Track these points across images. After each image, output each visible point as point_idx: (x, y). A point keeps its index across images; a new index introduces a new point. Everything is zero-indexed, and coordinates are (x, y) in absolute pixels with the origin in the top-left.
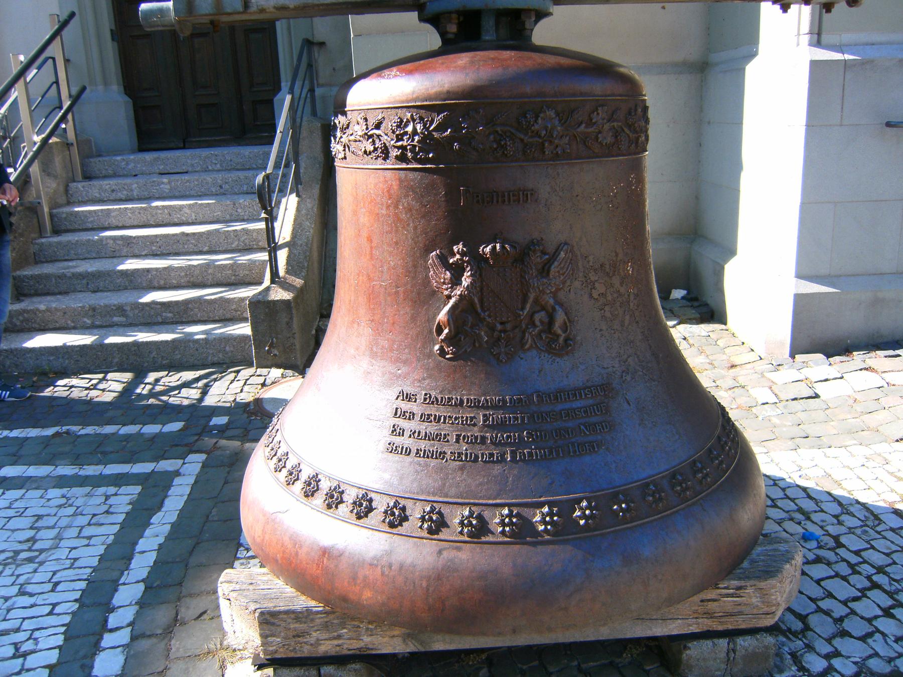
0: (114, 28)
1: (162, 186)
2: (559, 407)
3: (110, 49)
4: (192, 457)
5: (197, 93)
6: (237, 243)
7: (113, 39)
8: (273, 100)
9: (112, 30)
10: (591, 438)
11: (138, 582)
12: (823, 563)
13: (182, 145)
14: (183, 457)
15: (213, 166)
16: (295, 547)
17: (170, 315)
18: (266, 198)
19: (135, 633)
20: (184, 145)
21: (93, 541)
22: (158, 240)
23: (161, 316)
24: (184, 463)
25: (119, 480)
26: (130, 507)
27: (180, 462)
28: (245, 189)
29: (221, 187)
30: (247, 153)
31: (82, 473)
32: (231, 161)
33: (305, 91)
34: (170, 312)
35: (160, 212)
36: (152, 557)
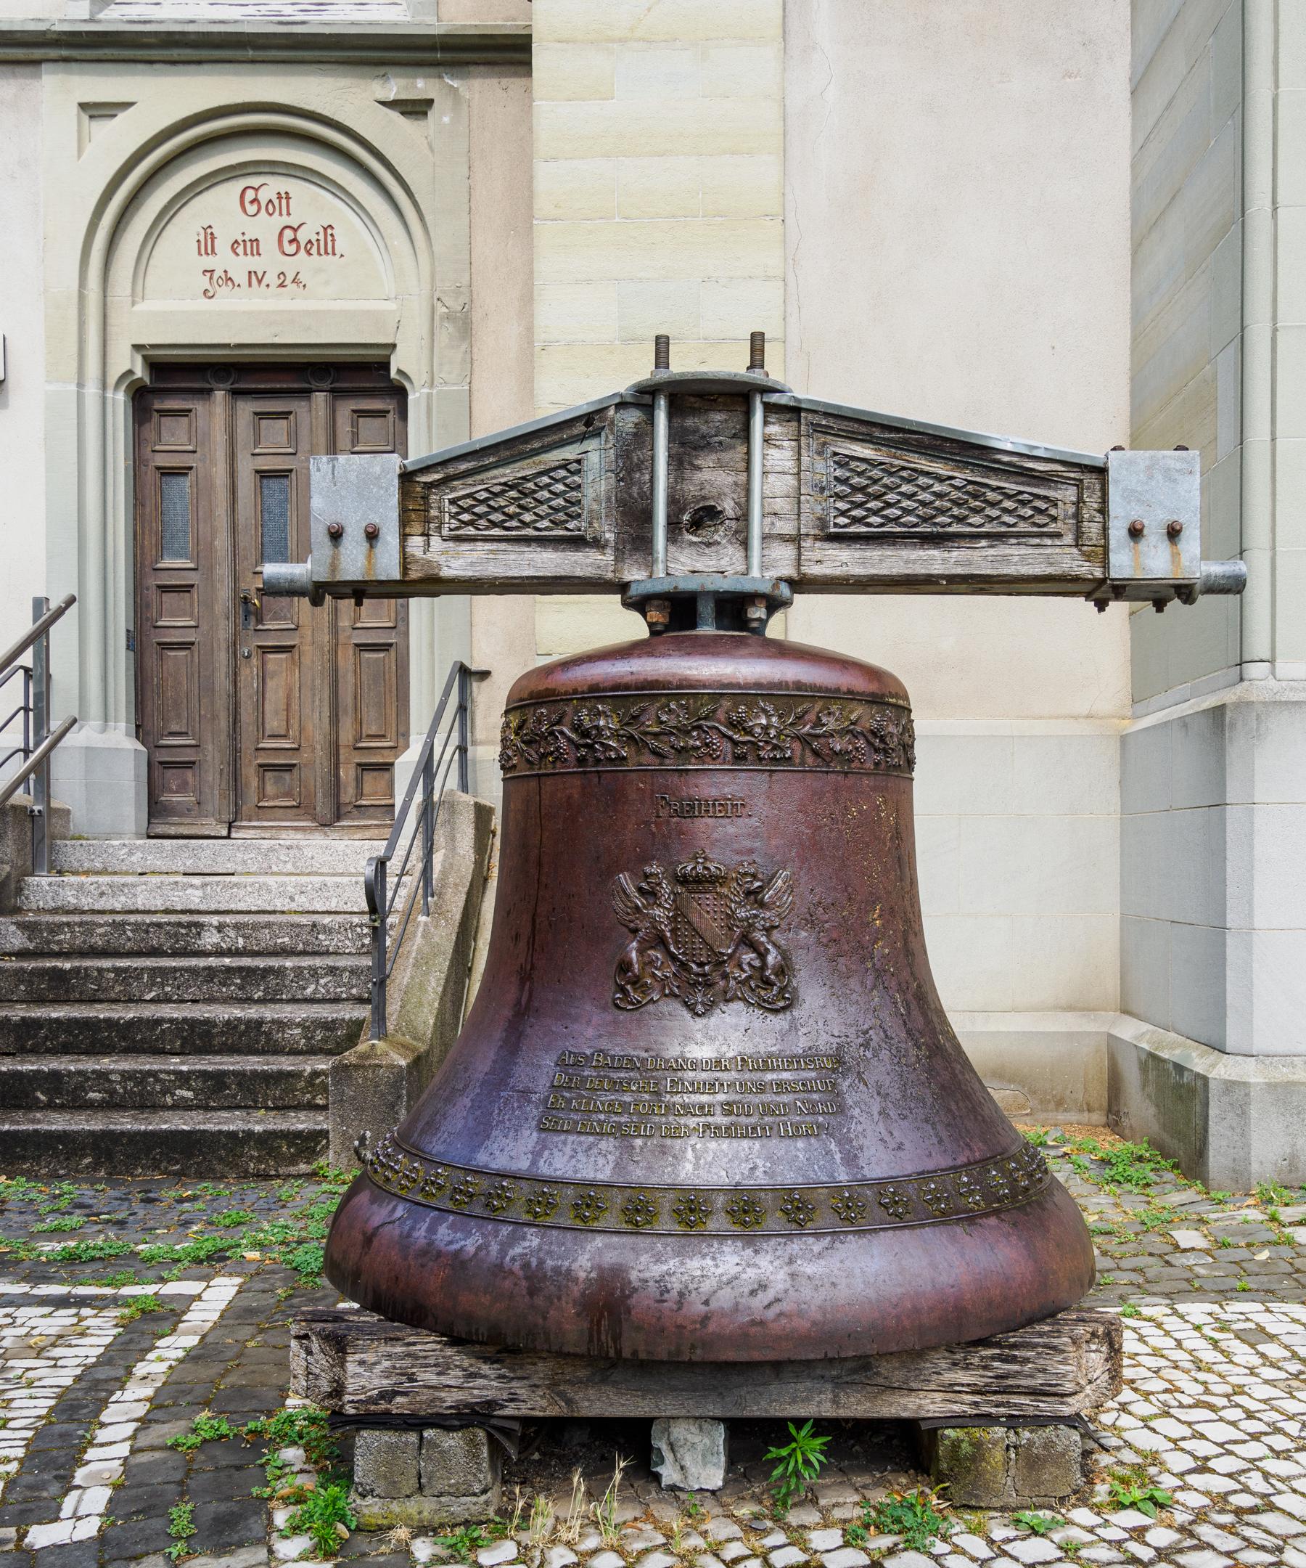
0: (132, 629)
3: (121, 660)
5: (261, 745)
6: (313, 986)
7: (128, 648)
8: (392, 764)
9: (128, 631)
12: (645, 617)
14: (207, 1278)
15: (281, 865)
16: (406, 1259)
17: (190, 1094)
20: (229, 832)
21: (60, 1363)
23: (173, 1094)
24: (208, 1286)
25: (98, 1303)
29: (292, 899)
31: (35, 1292)
33: (450, 750)
34: (188, 1089)
35: (183, 931)
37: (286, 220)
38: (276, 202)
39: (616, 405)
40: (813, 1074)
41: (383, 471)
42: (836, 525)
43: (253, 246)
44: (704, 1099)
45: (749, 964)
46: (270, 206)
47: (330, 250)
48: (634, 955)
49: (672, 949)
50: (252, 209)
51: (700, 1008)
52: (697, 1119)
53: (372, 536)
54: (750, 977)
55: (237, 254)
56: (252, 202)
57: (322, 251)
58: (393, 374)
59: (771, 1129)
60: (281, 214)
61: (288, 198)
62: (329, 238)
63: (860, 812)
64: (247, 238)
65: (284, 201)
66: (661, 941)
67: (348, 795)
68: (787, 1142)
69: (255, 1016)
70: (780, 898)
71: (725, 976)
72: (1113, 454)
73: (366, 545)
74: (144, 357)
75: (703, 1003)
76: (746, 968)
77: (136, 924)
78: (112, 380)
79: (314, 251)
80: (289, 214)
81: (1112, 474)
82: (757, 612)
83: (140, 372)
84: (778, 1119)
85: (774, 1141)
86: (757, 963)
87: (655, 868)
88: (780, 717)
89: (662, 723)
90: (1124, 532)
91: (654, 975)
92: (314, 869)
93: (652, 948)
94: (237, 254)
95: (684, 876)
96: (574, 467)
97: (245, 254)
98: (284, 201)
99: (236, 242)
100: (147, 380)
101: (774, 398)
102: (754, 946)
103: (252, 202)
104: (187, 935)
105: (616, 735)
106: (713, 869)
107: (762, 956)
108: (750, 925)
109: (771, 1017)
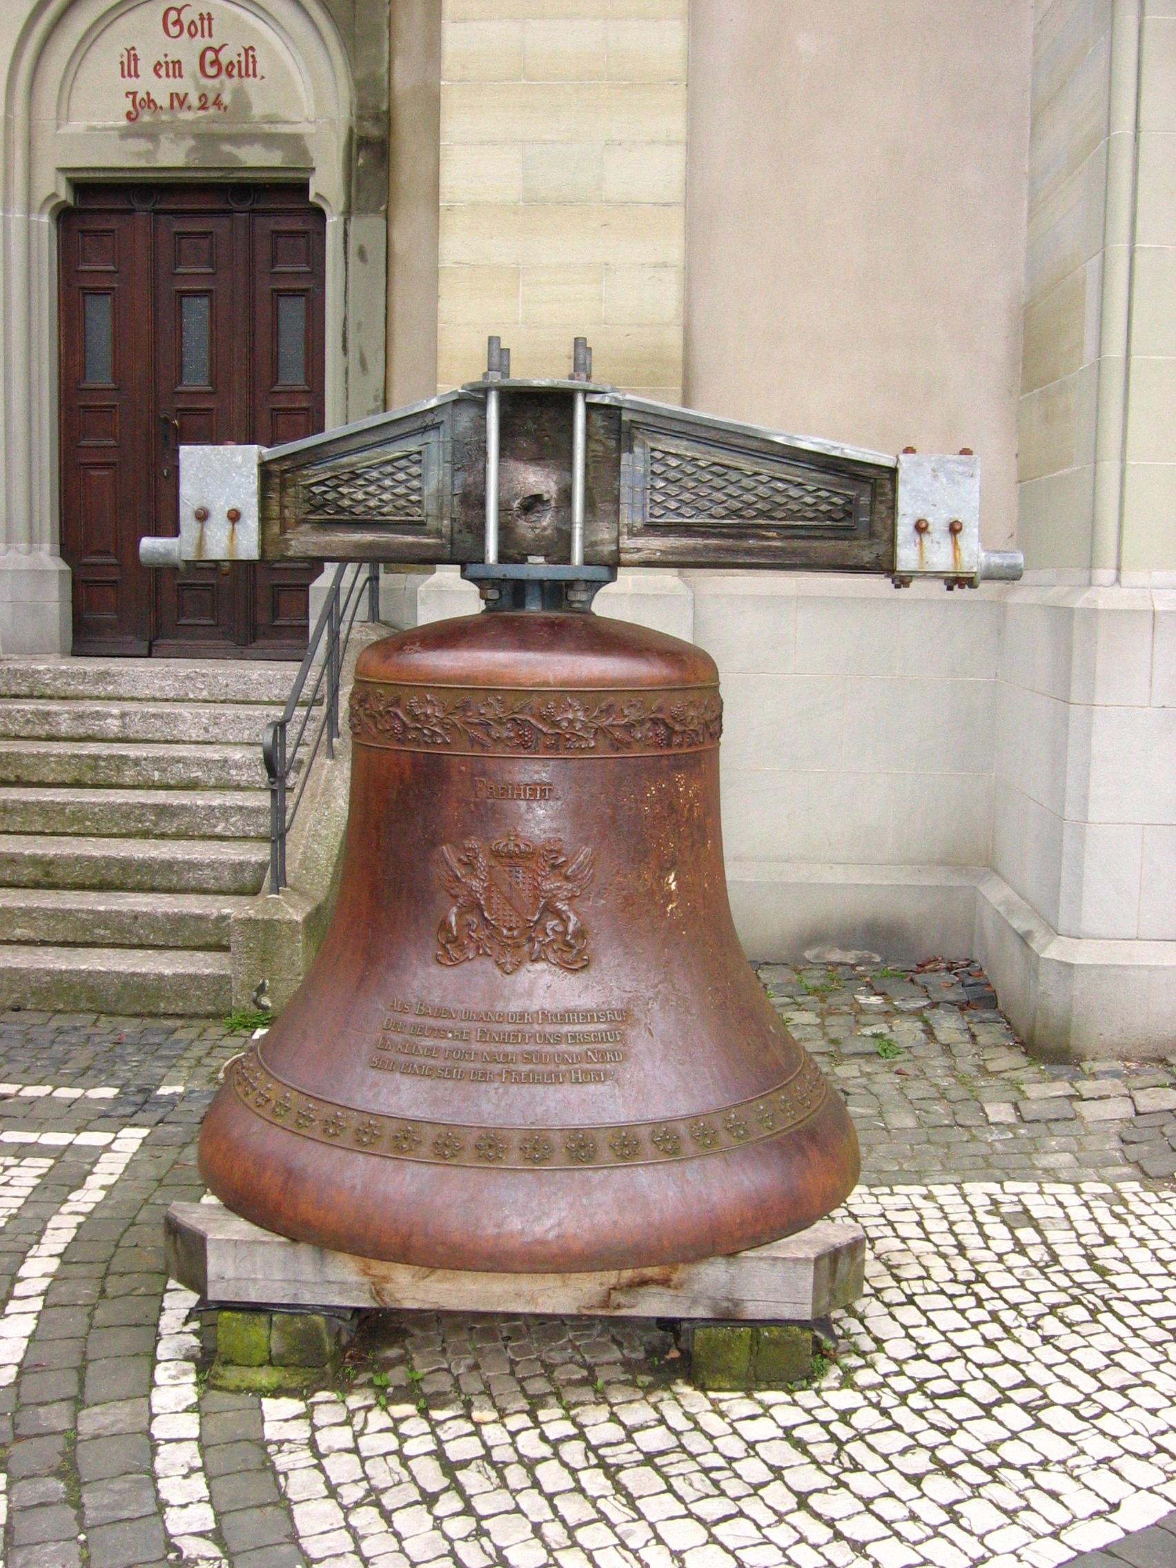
1: (109, 721)
2: (566, 1028)
4: (126, 1132)
8: (307, 586)
10: (598, 1066)
11: (51, 1256)
13: (145, 652)
18: (413, 545)
19: (48, 1302)
22: (96, 810)
25: (22, 1151)
26: (39, 1181)
27: (111, 1136)
28: (246, 736)
29: (206, 730)
30: (255, 676)
32: (227, 685)
35: (103, 764)
36: (68, 1235)
37: (208, 42)
38: (198, 23)
39: (454, 401)
40: (603, 1027)
41: (244, 461)
42: (652, 515)
43: (176, 68)
44: (509, 1048)
45: (552, 929)
46: (193, 28)
47: (251, 72)
48: (453, 919)
49: (486, 914)
50: (174, 30)
51: (509, 968)
52: (500, 1066)
53: (234, 516)
54: (553, 941)
55: (159, 76)
56: (175, 24)
57: (243, 73)
58: (312, 197)
59: (564, 1076)
60: (203, 36)
61: (210, 19)
62: (250, 60)
63: (658, 790)
64: (169, 59)
65: (206, 23)
66: (476, 907)
67: (263, 617)
68: (579, 1086)
69: (167, 856)
70: (582, 871)
71: (531, 940)
72: (902, 457)
73: (229, 526)
74: (69, 180)
75: (512, 964)
76: (550, 933)
77: (59, 756)
78: (37, 204)
79: (235, 72)
80: (210, 35)
81: (901, 475)
82: (580, 596)
83: (65, 194)
84: (572, 1067)
85: (567, 1086)
86: (560, 929)
87: (473, 843)
88: (586, 710)
89: (482, 714)
90: (911, 528)
91: (471, 937)
92: (229, 697)
93: (467, 912)
94: (159, 76)
95: (498, 851)
96: (415, 457)
97: (168, 76)
98: (206, 23)
99: (159, 63)
100: (71, 201)
101: (596, 399)
102: (558, 914)
103: (175, 24)
104: (106, 767)
105: (441, 723)
106: (522, 847)
107: (564, 921)
108: (555, 896)
109: (569, 976)
